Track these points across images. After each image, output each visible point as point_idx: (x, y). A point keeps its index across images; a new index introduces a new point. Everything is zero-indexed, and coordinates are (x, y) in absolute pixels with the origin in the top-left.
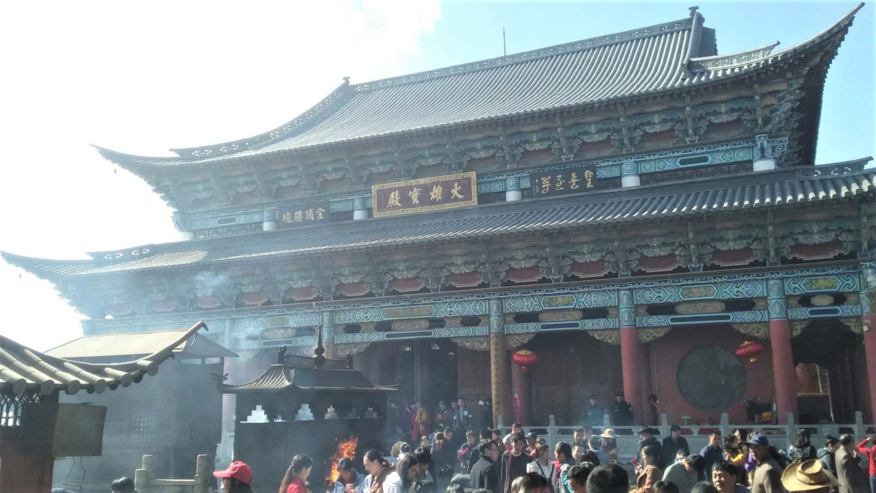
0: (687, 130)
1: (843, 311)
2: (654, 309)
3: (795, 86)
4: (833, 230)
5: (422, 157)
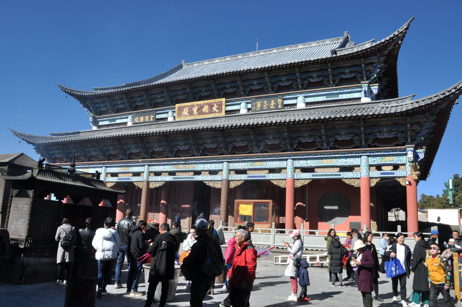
0: (329, 81)
1: (397, 173)
2: (238, 172)
3: (382, 60)
4: (394, 131)
5: (226, 88)
